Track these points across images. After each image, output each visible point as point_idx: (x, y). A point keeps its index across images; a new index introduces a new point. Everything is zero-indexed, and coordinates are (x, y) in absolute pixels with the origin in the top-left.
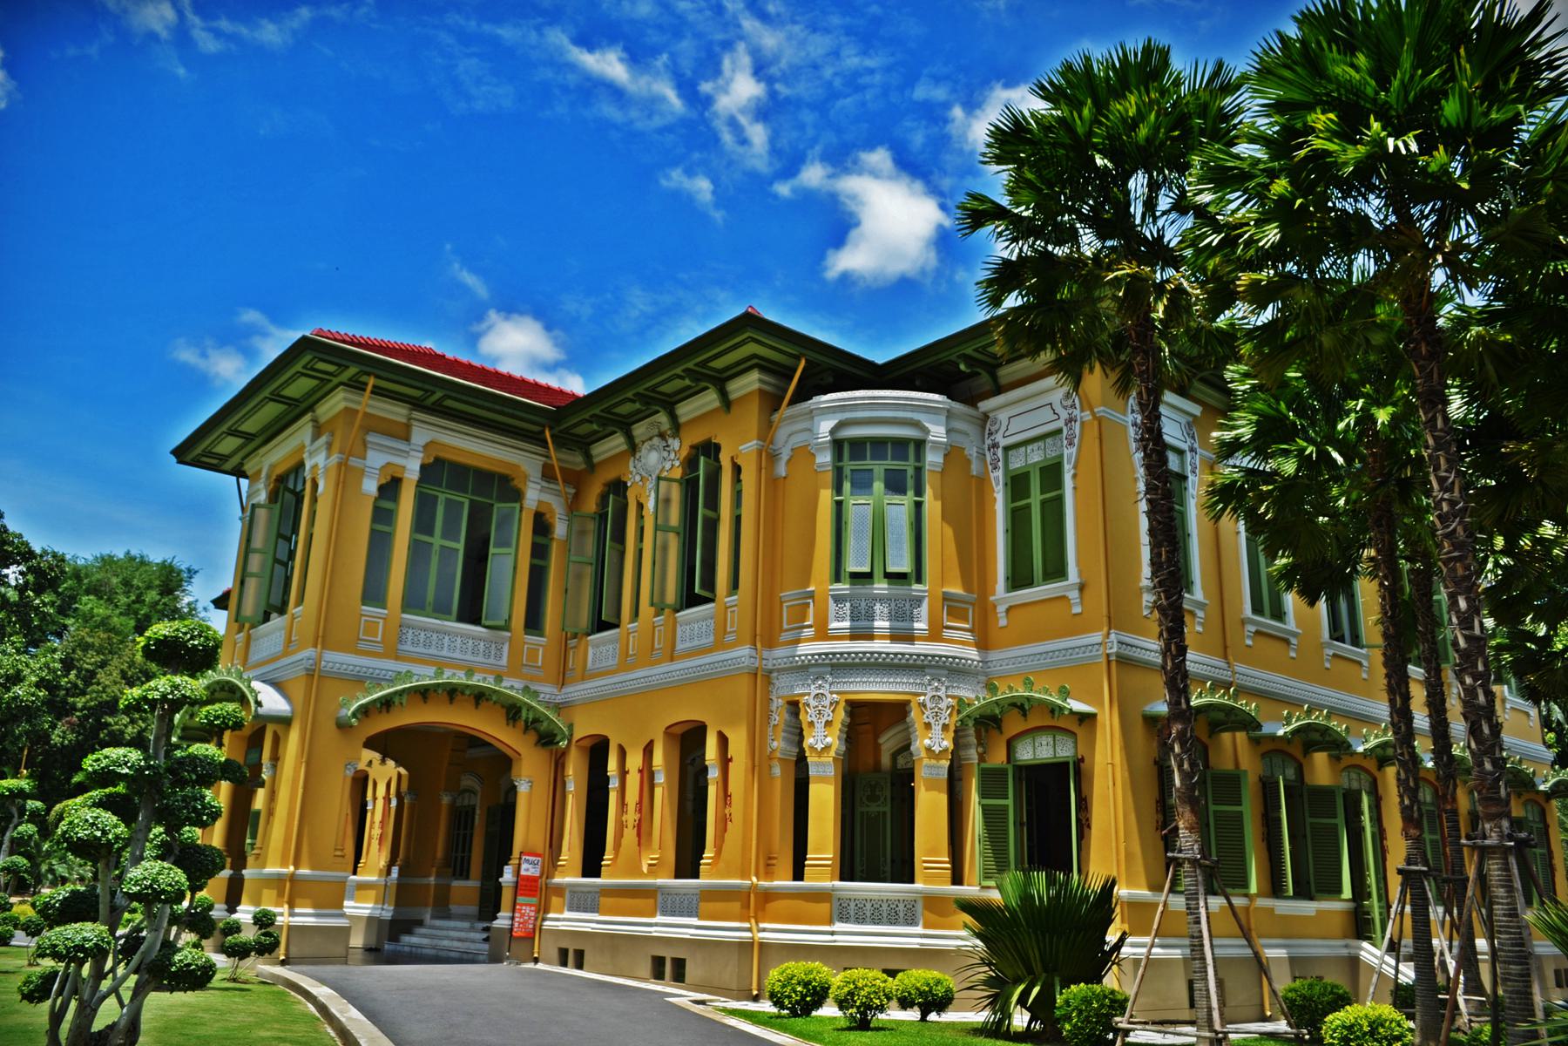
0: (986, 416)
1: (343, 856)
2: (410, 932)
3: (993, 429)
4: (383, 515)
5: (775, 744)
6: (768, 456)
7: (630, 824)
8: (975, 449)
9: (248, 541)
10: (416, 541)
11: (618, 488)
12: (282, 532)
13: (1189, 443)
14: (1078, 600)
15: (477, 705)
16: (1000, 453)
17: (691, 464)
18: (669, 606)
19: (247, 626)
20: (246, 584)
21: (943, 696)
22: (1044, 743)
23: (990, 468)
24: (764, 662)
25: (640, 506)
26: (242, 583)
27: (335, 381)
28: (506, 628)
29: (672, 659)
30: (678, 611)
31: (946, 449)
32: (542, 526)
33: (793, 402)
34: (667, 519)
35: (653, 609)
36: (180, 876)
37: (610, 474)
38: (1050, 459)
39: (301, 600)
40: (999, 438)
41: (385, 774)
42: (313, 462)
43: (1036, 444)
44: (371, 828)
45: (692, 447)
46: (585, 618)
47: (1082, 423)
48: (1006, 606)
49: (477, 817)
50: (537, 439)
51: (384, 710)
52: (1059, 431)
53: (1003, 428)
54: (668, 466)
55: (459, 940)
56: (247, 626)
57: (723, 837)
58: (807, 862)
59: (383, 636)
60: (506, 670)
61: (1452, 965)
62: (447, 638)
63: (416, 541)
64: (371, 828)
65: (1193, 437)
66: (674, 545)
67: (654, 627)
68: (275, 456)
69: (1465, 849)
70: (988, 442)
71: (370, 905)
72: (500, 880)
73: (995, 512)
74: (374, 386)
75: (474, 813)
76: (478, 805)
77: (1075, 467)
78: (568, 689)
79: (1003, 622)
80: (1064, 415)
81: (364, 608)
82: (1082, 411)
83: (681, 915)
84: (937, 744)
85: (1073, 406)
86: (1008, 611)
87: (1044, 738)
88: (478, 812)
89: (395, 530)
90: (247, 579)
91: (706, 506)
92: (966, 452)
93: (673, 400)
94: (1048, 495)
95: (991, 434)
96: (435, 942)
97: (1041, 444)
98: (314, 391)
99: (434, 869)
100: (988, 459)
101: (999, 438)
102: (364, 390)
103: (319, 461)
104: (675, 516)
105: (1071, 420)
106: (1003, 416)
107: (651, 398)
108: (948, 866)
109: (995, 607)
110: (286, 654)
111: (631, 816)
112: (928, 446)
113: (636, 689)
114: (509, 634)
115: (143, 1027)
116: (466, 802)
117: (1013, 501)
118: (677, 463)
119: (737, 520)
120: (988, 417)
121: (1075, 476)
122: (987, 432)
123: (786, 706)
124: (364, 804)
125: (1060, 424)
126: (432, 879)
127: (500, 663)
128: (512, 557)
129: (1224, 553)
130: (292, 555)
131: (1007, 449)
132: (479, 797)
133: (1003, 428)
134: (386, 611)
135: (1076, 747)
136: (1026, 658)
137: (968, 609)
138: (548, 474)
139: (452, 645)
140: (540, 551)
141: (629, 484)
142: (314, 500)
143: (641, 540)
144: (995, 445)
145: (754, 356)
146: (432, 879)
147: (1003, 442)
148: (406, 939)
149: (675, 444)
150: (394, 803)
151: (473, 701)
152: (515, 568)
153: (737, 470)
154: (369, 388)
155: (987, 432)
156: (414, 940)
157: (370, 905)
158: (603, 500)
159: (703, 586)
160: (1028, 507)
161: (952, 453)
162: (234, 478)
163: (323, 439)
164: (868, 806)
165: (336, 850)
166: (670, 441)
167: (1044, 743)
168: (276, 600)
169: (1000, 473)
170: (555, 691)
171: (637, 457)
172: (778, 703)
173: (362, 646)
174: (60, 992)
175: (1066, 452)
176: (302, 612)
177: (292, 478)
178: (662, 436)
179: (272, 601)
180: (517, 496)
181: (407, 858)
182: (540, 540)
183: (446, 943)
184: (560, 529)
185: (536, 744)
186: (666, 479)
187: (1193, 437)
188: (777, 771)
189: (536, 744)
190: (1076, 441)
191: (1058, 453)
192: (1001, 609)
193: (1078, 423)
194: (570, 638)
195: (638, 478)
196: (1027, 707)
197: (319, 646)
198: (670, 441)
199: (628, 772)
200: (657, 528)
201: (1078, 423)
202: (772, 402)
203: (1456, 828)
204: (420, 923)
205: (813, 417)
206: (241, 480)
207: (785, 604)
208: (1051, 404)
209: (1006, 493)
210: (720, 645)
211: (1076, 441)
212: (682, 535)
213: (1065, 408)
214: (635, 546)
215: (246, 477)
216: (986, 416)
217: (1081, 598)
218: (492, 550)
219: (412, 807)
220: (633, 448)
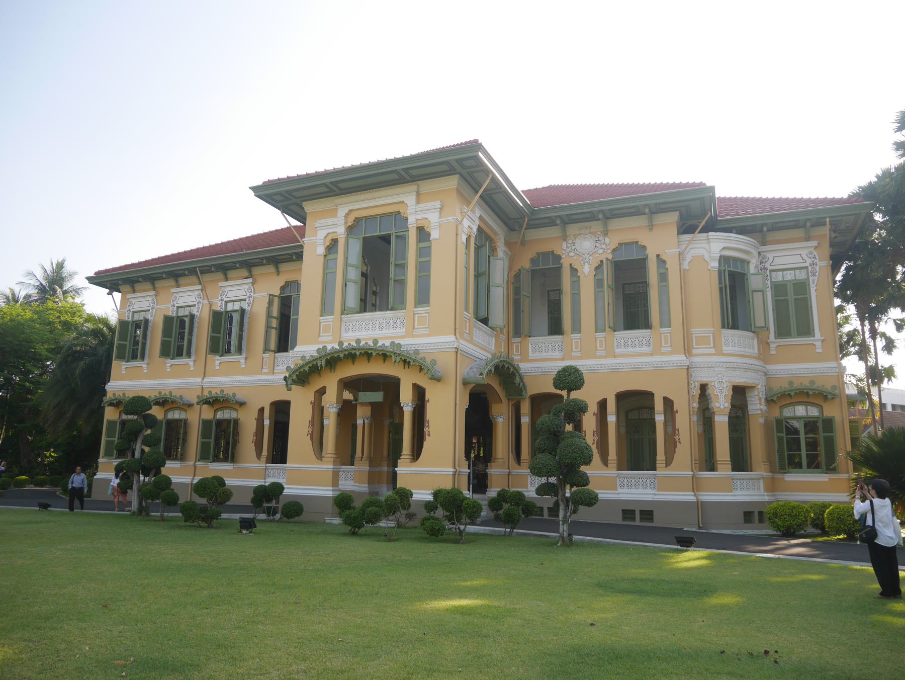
1: (504, 462)
15: (384, 360)
16: (131, 313)
33: (699, 233)
36: (10, 480)
38: (798, 280)
43: (788, 272)
57: (675, 450)
61: (262, 528)
80: (809, 261)
81: (661, 329)
84: (722, 405)
101: (767, 265)
108: (719, 463)
115: (891, 536)
151: (382, 358)
164: (652, 435)
190: (817, 274)
196: (411, 364)
203: (225, 436)
205: (709, 242)
208: (801, 255)
211: (817, 274)
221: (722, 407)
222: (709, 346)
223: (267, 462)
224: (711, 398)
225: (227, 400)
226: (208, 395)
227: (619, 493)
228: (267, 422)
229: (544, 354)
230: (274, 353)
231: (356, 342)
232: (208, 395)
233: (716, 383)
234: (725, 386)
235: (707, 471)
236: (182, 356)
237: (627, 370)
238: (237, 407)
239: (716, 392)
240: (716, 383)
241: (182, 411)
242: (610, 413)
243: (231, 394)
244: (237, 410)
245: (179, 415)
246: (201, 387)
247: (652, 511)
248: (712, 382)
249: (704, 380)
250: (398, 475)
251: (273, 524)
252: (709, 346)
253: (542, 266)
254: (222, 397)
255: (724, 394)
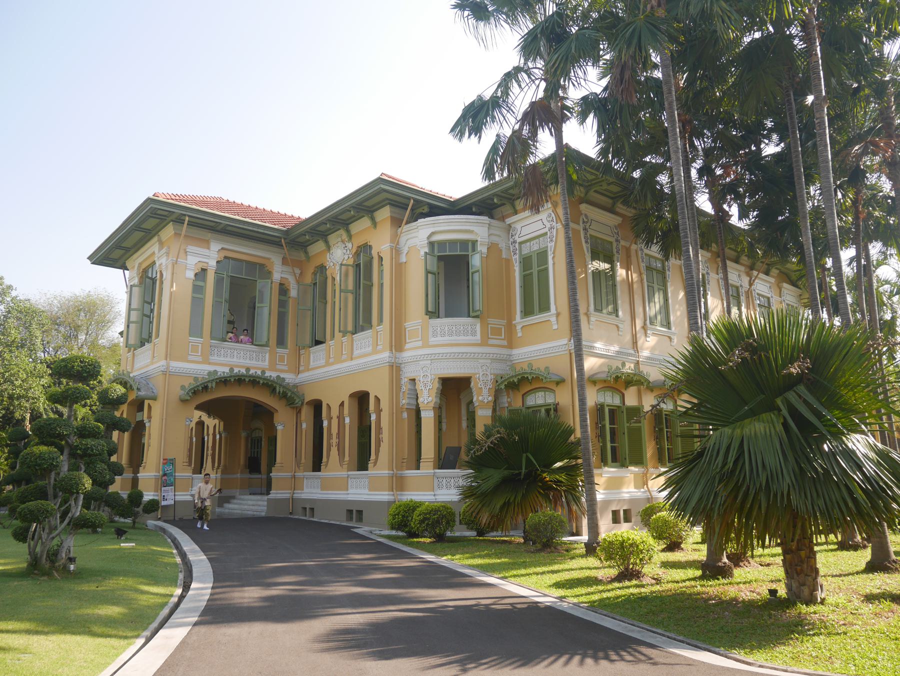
0: (510, 226)
2: (229, 502)
3: (514, 233)
4: (198, 289)
5: (404, 401)
6: (396, 250)
7: (334, 444)
8: (504, 244)
9: (130, 304)
10: (446, 243)
11: (322, 269)
12: (146, 300)
13: (615, 237)
14: (556, 322)
16: (517, 245)
17: (357, 254)
18: (349, 332)
19: (132, 349)
20: (130, 327)
21: (489, 374)
22: (540, 396)
23: (512, 254)
24: (397, 359)
25: (334, 279)
26: (128, 326)
27: (169, 219)
28: (266, 345)
29: (352, 359)
30: (354, 334)
31: (488, 245)
32: (283, 290)
33: (406, 224)
34: (347, 286)
35: (341, 334)
37: (316, 263)
39: (158, 336)
40: (516, 238)
41: (211, 422)
42: (160, 262)
44: (207, 450)
45: (358, 247)
46: (308, 339)
47: (557, 230)
48: (521, 326)
49: (263, 442)
50: (279, 245)
51: (204, 391)
52: (546, 234)
53: (519, 233)
54: (346, 257)
55: (253, 505)
56: (132, 349)
58: (432, 460)
59: (202, 352)
60: (268, 367)
62: (236, 352)
63: (446, 243)
64: (207, 450)
65: (618, 234)
66: (351, 298)
67: (342, 343)
68: (138, 260)
69: (178, 498)
70: (511, 240)
71: (152, 493)
72: (271, 474)
73: (515, 277)
74: (188, 221)
75: (261, 440)
76: (263, 437)
77: (554, 253)
78: (300, 376)
79: (520, 335)
80: (548, 225)
81: (190, 338)
82: (557, 223)
83: (375, 491)
85: (552, 221)
86: (522, 328)
87: (540, 393)
88: (263, 439)
89: (205, 297)
90: (131, 325)
91: (365, 279)
92: (500, 246)
93: (348, 222)
94: (545, 266)
95: (512, 236)
96: (242, 506)
97: (537, 240)
98: (158, 225)
99: (239, 471)
100: (512, 249)
101: (516, 238)
102: (184, 223)
103: (163, 262)
104: (351, 286)
105: (551, 228)
106: (518, 226)
107: (335, 222)
109: (516, 326)
110: (152, 363)
111: (334, 441)
112: (479, 243)
113: (360, 369)
114: (269, 349)
116: (257, 435)
117: (524, 271)
118: (351, 256)
119: (381, 286)
120: (511, 227)
121: (553, 258)
122: (511, 235)
123: (409, 381)
124: (203, 439)
125: (546, 230)
126: (239, 475)
127: (265, 364)
128: (268, 307)
129: (641, 293)
130: (152, 311)
131: (521, 243)
132: (263, 431)
133: (519, 233)
134: (202, 340)
135: (555, 397)
136: (536, 352)
137: (502, 328)
138: (285, 262)
139: (239, 355)
140: (282, 304)
141: (327, 267)
142: (161, 283)
143: (335, 298)
144: (515, 242)
145: (388, 199)
146: (239, 475)
147: (519, 240)
148: (226, 505)
149: (349, 245)
150: (218, 437)
152: (270, 314)
153: (381, 259)
154: (186, 222)
155: (511, 235)
156: (230, 506)
157: (152, 493)
158: (315, 274)
159: (364, 321)
160: (531, 274)
161: (492, 247)
162: (122, 270)
163: (164, 250)
165: (184, 462)
166: (347, 244)
167: (540, 396)
168: (145, 336)
169: (517, 257)
170: (294, 377)
171: (331, 253)
172: (405, 380)
173: (190, 358)
174: (33, 538)
175: (549, 245)
176: (160, 342)
177: (150, 270)
178: (343, 241)
179: (143, 337)
180: (268, 274)
181: (225, 466)
182: (283, 298)
183: (246, 507)
184: (293, 293)
185: (286, 406)
186: (345, 265)
187: (618, 234)
188: (405, 415)
189: (286, 406)
191: (545, 246)
192: (519, 327)
193: (555, 229)
194: (299, 348)
195: (332, 264)
197: (168, 359)
198: (347, 244)
199: (381, 410)
200: (341, 291)
201: (555, 229)
202: (397, 222)
204: (234, 497)
206: (125, 271)
207: (407, 329)
209: (520, 267)
210: (375, 352)
211: (554, 239)
212: (355, 294)
213: (549, 221)
214: (332, 300)
215: (128, 270)
216: (510, 226)
217: (557, 320)
218: (257, 305)
219: (226, 438)
220: (329, 248)
221: (486, 401)
222: (500, 337)
223: (348, 471)
224: (436, 393)
225: (537, 378)
226: (527, 368)
227: (348, 494)
228: (347, 420)
229: (363, 350)
230: (350, 335)
231: (246, 371)
232: (527, 368)
233: (481, 375)
234: (489, 379)
235: (439, 469)
236: (534, 313)
237: (545, 356)
238: (553, 387)
239: (480, 384)
240: (481, 375)
241: (547, 393)
242: (423, 408)
243: (542, 369)
244: (553, 391)
245: (544, 399)
246: (567, 352)
247: (362, 511)
248: (476, 374)
249: (412, 376)
250: (140, 480)
251: (544, 575)
252: (500, 337)
253: (449, 252)
254: (530, 373)
255: (488, 388)
